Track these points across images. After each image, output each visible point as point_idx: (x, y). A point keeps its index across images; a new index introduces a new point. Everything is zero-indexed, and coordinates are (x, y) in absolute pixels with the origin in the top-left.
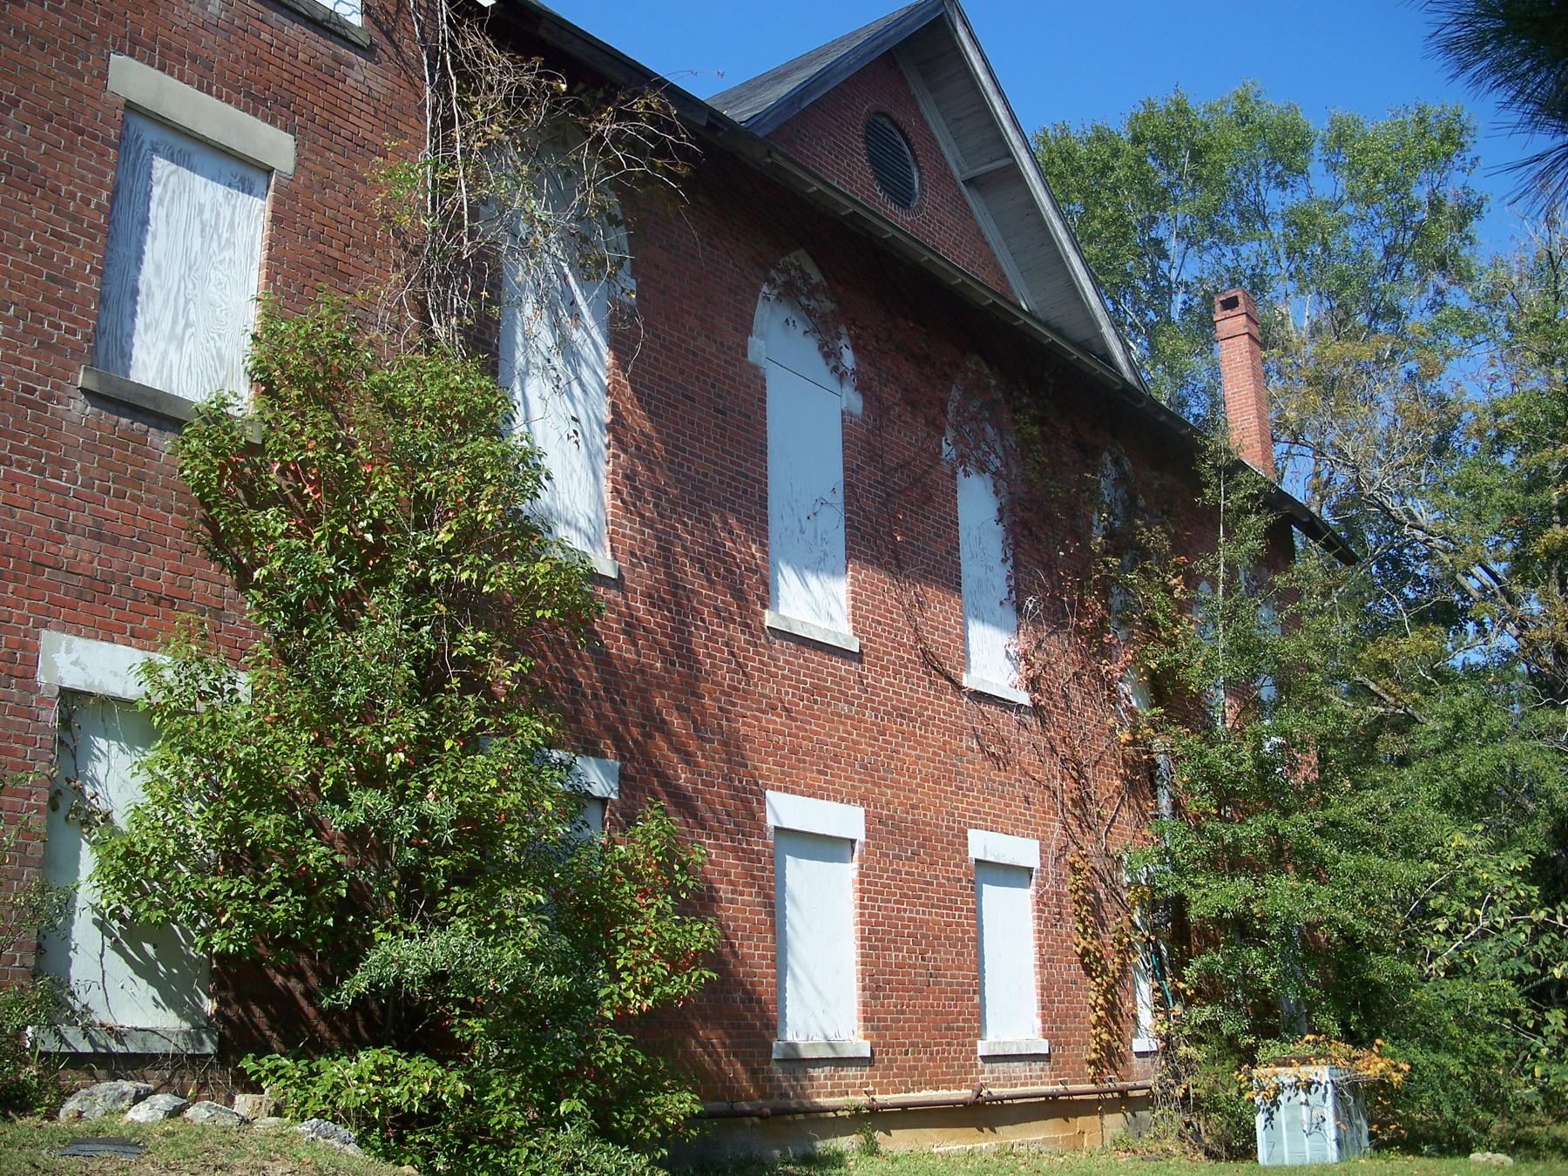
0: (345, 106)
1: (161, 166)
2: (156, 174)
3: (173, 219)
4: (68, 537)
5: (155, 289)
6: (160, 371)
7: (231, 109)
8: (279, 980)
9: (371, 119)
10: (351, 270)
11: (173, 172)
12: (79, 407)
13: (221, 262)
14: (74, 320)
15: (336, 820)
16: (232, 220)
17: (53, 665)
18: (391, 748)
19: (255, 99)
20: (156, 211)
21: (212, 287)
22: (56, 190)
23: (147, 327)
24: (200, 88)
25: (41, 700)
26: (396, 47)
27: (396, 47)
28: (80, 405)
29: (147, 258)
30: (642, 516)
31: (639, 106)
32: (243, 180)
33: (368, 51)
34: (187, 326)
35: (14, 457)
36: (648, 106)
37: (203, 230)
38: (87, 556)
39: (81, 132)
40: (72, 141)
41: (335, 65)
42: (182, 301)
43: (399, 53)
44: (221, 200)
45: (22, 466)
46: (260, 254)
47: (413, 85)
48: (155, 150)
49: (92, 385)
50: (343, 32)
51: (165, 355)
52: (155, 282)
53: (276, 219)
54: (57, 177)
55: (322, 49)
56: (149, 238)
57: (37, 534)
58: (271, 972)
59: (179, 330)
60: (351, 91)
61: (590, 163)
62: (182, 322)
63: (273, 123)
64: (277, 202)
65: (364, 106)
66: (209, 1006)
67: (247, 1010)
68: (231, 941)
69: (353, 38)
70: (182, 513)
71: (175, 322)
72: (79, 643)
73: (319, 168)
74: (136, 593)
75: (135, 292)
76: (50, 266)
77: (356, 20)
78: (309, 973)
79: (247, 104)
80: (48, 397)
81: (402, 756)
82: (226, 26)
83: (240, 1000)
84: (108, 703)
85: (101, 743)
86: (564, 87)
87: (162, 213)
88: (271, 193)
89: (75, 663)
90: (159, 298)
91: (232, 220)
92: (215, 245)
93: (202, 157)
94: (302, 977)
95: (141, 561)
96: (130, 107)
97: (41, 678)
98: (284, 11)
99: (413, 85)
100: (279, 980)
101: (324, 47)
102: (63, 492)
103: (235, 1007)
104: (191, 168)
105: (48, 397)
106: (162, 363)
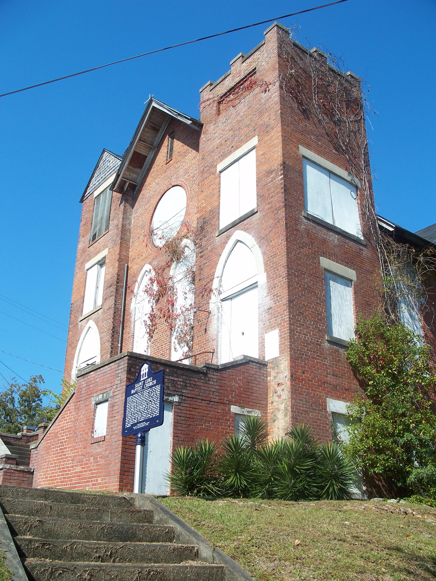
0: (364, 262)
1: (331, 283)
2: (331, 285)
3: (335, 295)
4: (329, 376)
5: (334, 313)
6: (338, 334)
7: (343, 266)
8: (377, 482)
9: (369, 264)
10: (371, 304)
11: (334, 284)
12: (327, 345)
13: (345, 305)
14: (323, 324)
15: (401, 441)
16: (346, 294)
17: (329, 407)
18: (411, 423)
19: (347, 263)
20: (332, 294)
21: (345, 312)
22: (315, 292)
23: (334, 323)
24: (336, 262)
25: (328, 415)
26: (371, 243)
27: (371, 243)
28: (327, 344)
29: (332, 306)
30: (434, 361)
31: (428, 253)
32: (347, 284)
33: (365, 246)
34: (342, 322)
35: (317, 357)
36: (431, 252)
37: (341, 298)
38: (332, 380)
39: (317, 277)
40: (316, 280)
41: (360, 251)
42: (340, 316)
43: (372, 245)
44: (343, 289)
45: (319, 360)
46: (352, 302)
47: (376, 253)
48: (330, 279)
49: (329, 339)
50: (361, 242)
51: (338, 329)
52: (334, 312)
53: (355, 293)
54: (315, 289)
55: (357, 247)
56: (332, 301)
57: (324, 375)
58: (375, 480)
59: (340, 323)
60: (364, 257)
61: (419, 269)
62: (340, 321)
63: (351, 268)
64: (355, 289)
65: (367, 261)
66: (364, 488)
67: (372, 489)
68: (380, 470)
69: (363, 243)
70: (348, 368)
71: (339, 321)
72: (334, 401)
73: (361, 278)
74: (342, 388)
75: (331, 315)
76: (317, 311)
77: (362, 238)
78: (383, 481)
79: (345, 264)
80: (321, 343)
81: (414, 425)
82: (339, 245)
83: (371, 487)
84: (340, 415)
85: (339, 424)
86: (414, 251)
87: (333, 294)
88: (353, 286)
89: (333, 406)
90: (335, 316)
91: (346, 294)
92: (344, 301)
93: (339, 279)
94: (381, 482)
95: (342, 380)
96: (325, 269)
97: (328, 410)
98: (349, 239)
99: (376, 253)
100: (377, 482)
101: (357, 246)
102: (326, 365)
103: (370, 488)
104: (337, 283)
105: (321, 343)
106: (338, 332)
